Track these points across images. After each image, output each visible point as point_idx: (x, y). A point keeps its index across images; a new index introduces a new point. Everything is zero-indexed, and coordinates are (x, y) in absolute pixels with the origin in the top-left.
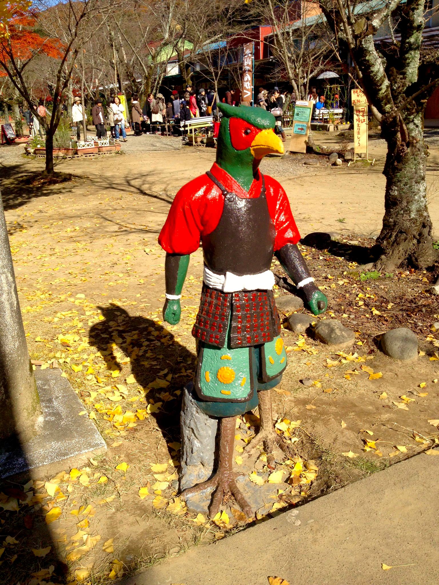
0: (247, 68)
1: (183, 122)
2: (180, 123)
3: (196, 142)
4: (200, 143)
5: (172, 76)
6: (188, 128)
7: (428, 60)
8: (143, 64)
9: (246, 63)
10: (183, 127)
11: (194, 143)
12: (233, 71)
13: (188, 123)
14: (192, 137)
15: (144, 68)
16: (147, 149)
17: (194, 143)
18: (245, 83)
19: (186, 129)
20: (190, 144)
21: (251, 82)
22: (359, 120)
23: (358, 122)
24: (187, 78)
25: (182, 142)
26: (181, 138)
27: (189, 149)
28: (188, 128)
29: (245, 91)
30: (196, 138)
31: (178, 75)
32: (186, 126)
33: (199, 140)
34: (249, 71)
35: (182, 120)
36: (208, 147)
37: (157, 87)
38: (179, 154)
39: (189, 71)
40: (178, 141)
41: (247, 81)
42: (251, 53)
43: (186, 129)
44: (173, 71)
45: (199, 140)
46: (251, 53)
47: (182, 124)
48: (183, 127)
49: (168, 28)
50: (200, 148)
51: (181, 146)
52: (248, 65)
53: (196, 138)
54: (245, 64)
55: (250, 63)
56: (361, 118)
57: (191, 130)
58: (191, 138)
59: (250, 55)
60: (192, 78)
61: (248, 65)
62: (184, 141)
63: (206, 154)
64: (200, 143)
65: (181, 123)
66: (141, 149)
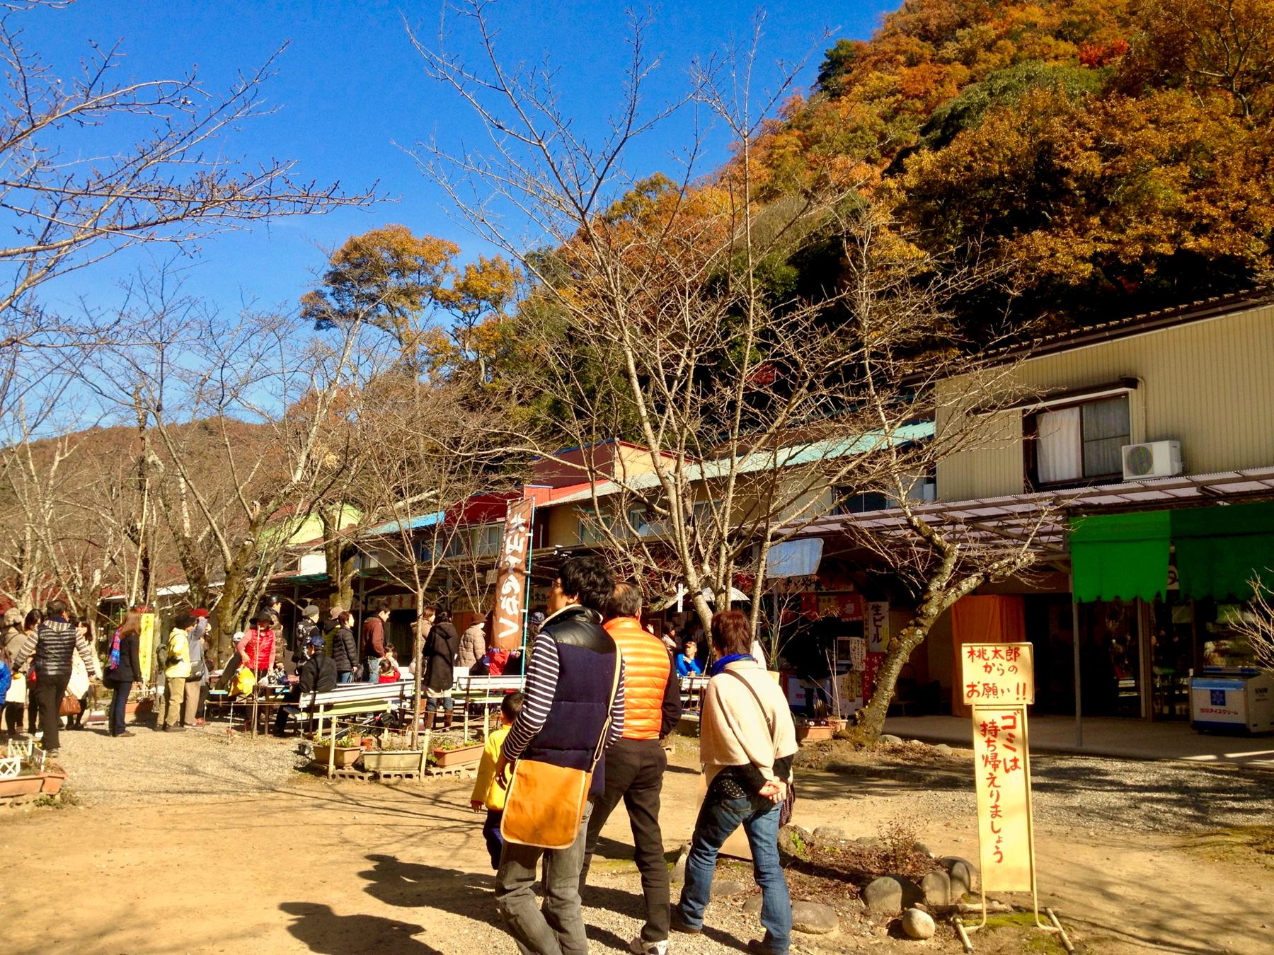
0: (513, 561)
1: (309, 697)
2: (298, 701)
3: (339, 765)
4: (349, 769)
5: (307, 577)
6: (320, 716)
7: (1000, 573)
8: (222, 539)
9: (509, 548)
10: (305, 710)
11: (332, 767)
12: (462, 573)
13: (322, 699)
14: (328, 748)
15: (225, 548)
16: (168, 783)
17: (332, 767)
18: (504, 600)
19: (315, 716)
20: (316, 769)
21: (521, 596)
22: (994, 762)
23: (989, 768)
24: (343, 582)
25: (293, 760)
26: (293, 743)
27: (313, 787)
28: (320, 716)
29: (502, 620)
30: (339, 754)
31: (323, 575)
32: (316, 709)
33: (349, 757)
34: (516, 570)
35: (307, 692)
36: (377, 896)
37: (253, 598)
38: (267, 812)
39: (349, 567)
40: (280, 754)
41: (509, 595)
42: (525, 525)
43: (315, 716)
44: (313, 565)
45: (349, 757)
46: (525, 525)
47: (304, 701)
48: (305, 710)
49: (304, 458)
50: (346, 786)
51: (288, 773)
52: (514, 553)
53: (339, 754)
54: (508, 551)
55: (521, 548)
56: (1005, 754)
57: (327, 723)
58: (323, 751)
59: (522, 529)
60: (355, 583)
61: (514, 553)
62: (300, 758)
63: (366, 818)
64: (353, 771)
65: (302, 698)
66: (145, 783)
